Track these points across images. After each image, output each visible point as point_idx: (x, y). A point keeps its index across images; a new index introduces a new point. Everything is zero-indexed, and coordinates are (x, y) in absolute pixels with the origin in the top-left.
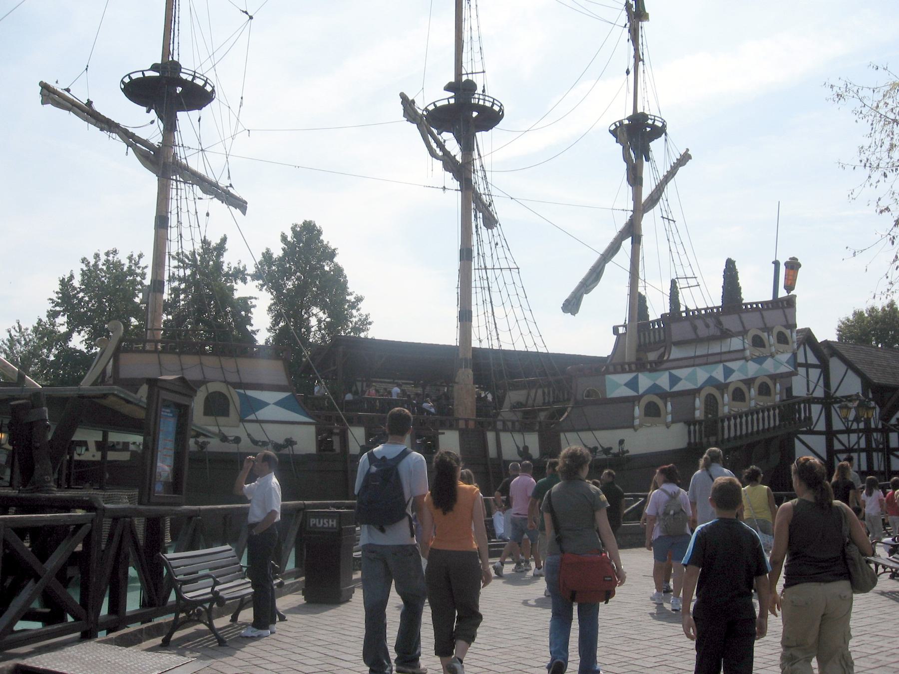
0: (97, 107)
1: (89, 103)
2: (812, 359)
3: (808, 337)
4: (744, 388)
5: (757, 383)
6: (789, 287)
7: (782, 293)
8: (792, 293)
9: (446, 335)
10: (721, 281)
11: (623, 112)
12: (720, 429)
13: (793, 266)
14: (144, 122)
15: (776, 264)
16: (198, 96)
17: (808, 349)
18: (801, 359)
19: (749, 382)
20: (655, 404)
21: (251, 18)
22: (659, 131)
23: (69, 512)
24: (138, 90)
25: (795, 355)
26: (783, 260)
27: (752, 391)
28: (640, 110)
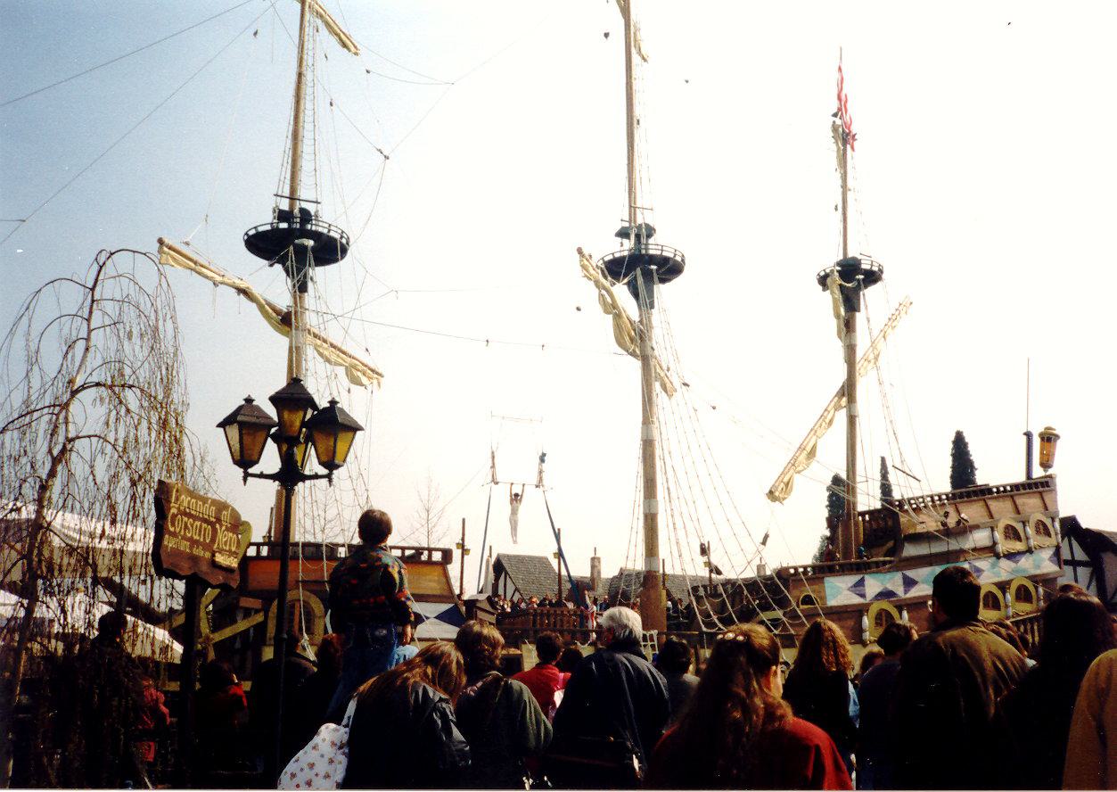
0: (264, 473)
1: (262, 473)
2: (1080, 555)
3: (1071, 527)
4: (999, 594)
5: (1014, 587)
6: (1046, 464)
7: (1038, 472)
8: (1050, 471)
9: (619, 555)
10: (949, 461)
11: (829, 260)
12: (1036, 634)
13: (1049, 438)
14: (272, 282)
15: (1028, 435)
16: (330, 250)
17: (1075, 544)
18: (1066, 555)
19: (1003, 586)
20: (1023, 586)
21: (387, 158)
22: (872, 277)
23: (984, 600)
24: (264, 245)
25: (1058, 548)
26: (1036, 432)
27: (1008, 596)
28: (850, 255)
